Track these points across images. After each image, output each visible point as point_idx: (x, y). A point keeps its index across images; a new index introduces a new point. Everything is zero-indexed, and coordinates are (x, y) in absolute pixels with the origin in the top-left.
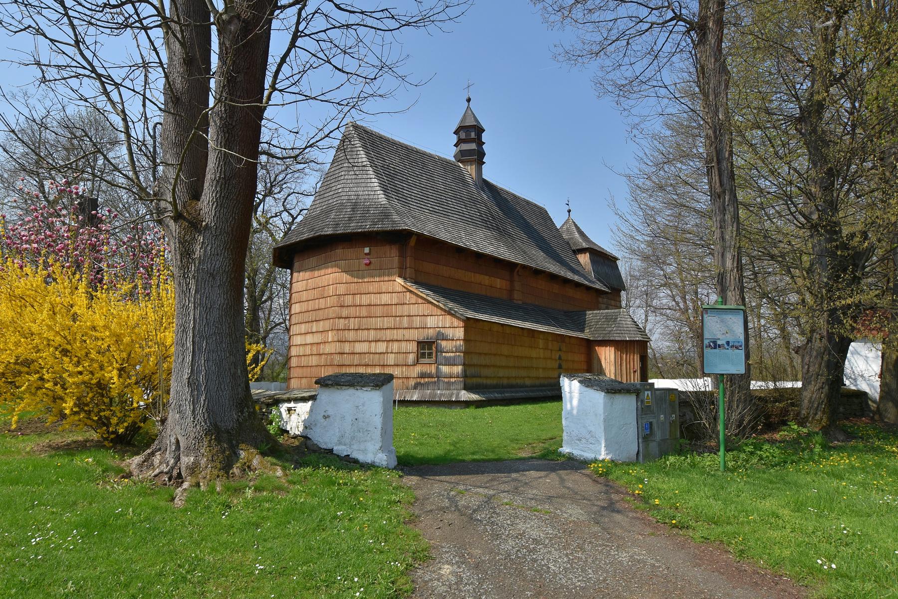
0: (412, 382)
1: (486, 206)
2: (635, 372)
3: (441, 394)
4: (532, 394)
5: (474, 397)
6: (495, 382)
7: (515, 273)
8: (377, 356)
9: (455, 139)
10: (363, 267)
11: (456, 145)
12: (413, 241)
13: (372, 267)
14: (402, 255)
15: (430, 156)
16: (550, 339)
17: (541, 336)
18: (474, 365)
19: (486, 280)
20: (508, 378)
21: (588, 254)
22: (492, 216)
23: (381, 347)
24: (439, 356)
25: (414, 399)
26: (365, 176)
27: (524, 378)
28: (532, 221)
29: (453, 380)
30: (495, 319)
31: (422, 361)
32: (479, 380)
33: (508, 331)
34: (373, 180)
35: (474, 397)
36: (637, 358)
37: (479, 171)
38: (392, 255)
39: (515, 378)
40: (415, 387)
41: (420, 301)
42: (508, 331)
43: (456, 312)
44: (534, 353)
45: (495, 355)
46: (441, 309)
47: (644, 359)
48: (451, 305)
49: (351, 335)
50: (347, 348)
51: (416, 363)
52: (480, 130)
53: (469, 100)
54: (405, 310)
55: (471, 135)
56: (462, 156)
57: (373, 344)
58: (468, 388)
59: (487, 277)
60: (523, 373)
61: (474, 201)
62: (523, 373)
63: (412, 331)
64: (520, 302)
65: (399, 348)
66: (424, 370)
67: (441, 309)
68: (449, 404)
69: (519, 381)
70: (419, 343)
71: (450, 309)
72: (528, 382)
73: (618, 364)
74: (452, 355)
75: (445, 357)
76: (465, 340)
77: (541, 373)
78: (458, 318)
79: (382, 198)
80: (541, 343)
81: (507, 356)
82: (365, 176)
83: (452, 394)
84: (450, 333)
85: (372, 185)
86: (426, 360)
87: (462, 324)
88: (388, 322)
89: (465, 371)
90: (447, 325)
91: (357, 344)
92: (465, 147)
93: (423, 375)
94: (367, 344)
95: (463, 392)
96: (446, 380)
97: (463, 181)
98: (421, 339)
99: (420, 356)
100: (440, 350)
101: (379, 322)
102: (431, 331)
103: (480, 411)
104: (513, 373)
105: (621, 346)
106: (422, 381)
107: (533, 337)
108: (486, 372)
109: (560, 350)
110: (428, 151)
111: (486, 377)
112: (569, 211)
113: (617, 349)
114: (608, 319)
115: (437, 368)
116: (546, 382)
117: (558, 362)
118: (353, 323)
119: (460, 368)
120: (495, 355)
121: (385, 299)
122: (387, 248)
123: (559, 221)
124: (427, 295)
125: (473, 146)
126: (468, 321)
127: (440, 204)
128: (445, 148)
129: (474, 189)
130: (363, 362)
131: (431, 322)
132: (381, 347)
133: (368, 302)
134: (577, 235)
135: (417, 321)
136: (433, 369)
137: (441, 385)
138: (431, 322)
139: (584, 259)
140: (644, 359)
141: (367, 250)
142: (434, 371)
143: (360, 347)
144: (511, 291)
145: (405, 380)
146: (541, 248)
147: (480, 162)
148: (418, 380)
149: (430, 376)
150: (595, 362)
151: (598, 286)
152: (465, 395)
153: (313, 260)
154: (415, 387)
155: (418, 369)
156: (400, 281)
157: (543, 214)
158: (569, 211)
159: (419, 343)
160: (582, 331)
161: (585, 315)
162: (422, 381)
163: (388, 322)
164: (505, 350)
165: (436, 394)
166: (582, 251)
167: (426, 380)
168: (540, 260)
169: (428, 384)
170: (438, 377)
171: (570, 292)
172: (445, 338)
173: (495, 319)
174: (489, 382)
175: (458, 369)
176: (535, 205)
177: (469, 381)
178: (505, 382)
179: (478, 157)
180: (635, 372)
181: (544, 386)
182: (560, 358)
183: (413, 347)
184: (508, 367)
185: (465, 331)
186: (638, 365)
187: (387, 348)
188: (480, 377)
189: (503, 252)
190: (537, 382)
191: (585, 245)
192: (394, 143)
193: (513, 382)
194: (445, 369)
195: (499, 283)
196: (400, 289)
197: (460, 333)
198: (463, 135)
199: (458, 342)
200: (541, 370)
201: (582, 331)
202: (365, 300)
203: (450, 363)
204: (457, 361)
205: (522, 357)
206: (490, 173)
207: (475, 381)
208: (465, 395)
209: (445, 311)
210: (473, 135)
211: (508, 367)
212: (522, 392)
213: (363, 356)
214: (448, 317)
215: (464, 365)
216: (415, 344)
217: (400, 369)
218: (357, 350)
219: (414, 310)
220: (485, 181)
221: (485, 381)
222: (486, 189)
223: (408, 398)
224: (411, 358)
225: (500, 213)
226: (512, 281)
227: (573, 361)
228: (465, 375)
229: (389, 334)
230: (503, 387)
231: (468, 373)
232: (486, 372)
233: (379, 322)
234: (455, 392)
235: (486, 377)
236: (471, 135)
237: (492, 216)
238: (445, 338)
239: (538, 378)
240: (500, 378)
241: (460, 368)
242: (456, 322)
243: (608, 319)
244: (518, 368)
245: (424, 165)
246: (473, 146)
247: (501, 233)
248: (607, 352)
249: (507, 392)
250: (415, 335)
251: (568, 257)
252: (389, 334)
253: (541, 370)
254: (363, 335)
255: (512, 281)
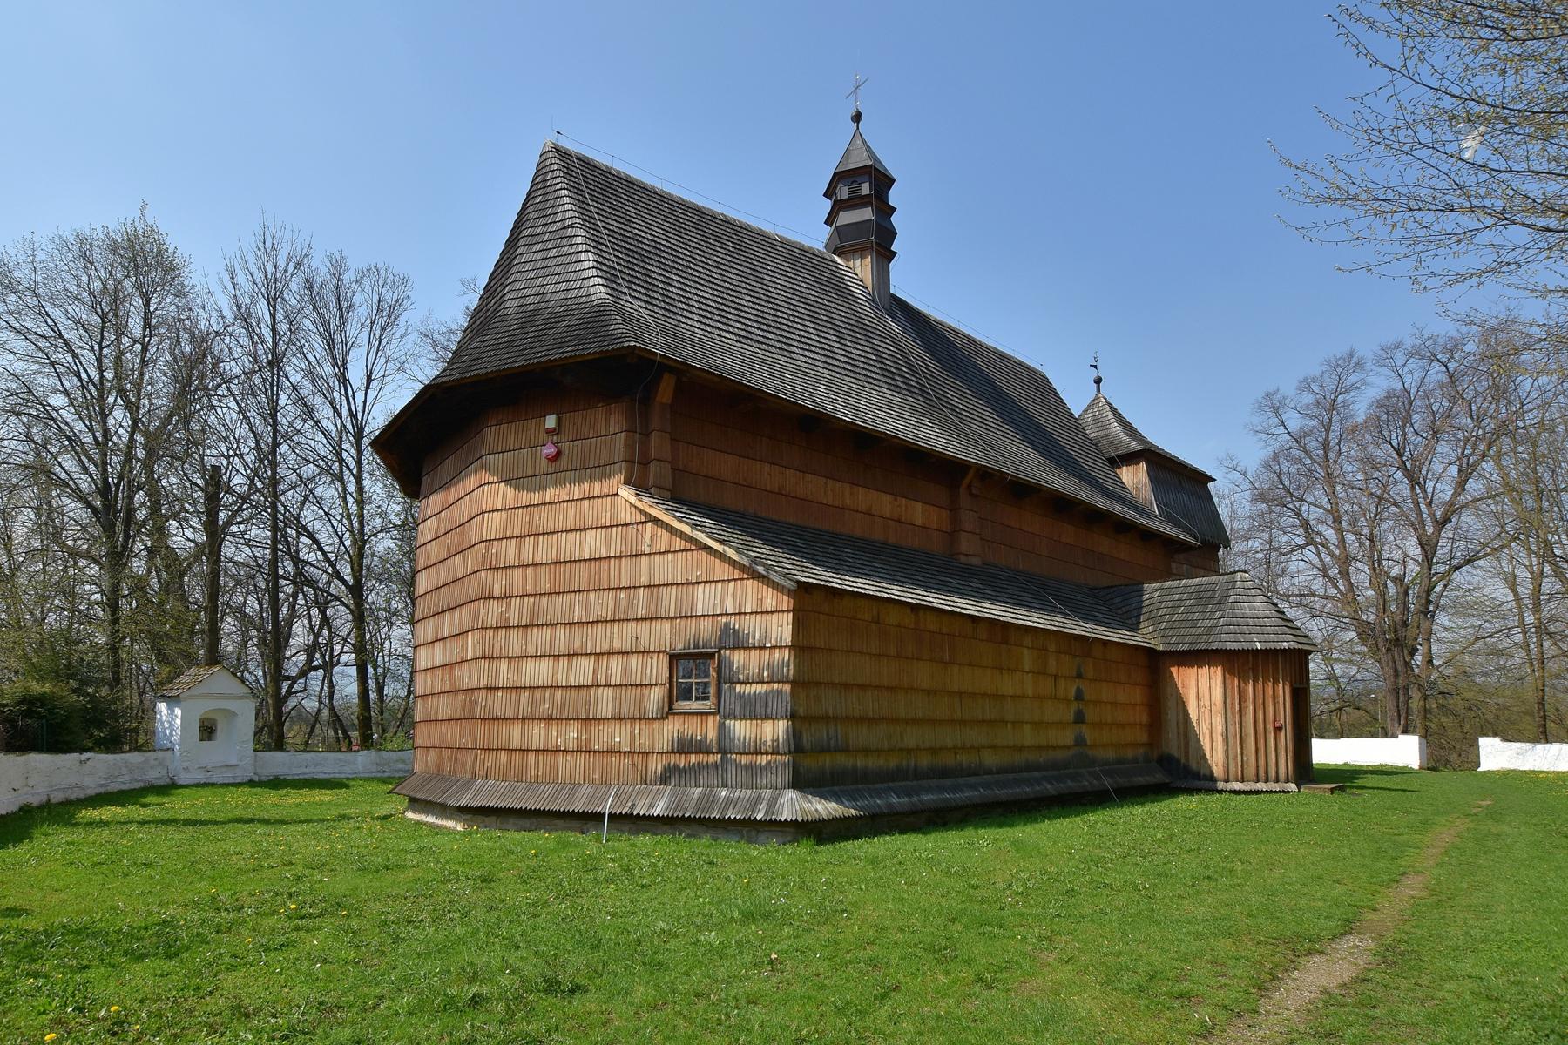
0: (656, 765)
1: (895, 343)
2: (1278, 729)
3: (729, 800)
4: (1000, 793)
5: (823, 808)
6: (893, 763)
7: (962, 490)
8: (573, 693)
9: (827, 205)
10: (543, 466)
11: (829, 222)
12: (665, 391)
13: (563, 463)
14: (639, 429)
15: (761, 236)
16: (1052, 648)
17: (1028, 641)
18: (826, 719)
19: (884, 503)
20: (934, 751)
21: (1143, 466)
22: (910, 366)
23: (582, 671)
24: (726, 695)
25: (658, 810)
26: (566, 250)
27: (980, 749)
28: (1013, 390)
29: (762, 760)
30: (894, 592)
31: (684, 706)
32: (842, 760)
33: (931, 623)
34: (583, 256)
35: (823, 808)
36: (1283, 692)
37: (882, 275)
38: (610, 429)
39: (954, 750)
40: (664, 779)
41: (678, 544)
42: (931, 623)
43: (768, 568)
44: (1008, 685)
45: (891, 689)
46: (733, 563)
47: (1300, 696)
48: (760, 550)
49: (513, 642)
50: (503, 674)
51: (668, 712)
52: (883, 181)
53: (857, 118)
54: (641, 571)
55: (863, 192)
56: (846, 241)
57: (563, 663)
58: (802, 782)
59: (886, 498)
60: (974, 736)
61: (866, 332)
62: (974, 736)
63: (657, 626)
64: (976, 561)
65: (626, 672)
66: (688, 732)
67: (733, 563)
68: (749, 828)
69: (964, 759)
70: (674, 658)
71: (754, 560)
72: (991, 760)
73: (1234, 710)
74: (760, 688)
75: (741, 696)
76: (798, 647)
77: (1028, 737)
78: (777, 587)
79: (598, 290)
80: (1028, 659)
81: (929, 692)
82: (566, 250)
83: (759, 800)
84: (754, 627)
85: (579, 266)
86: (693, 706)
87: (786, 602)
88: (600, 605)
89: (795, 739)
90: (747, 604)
91: (526, 665)
92: (846, 218)
93: (684, 746)
94: (547, 664)
95: (790, 794)
96: (745, 760)
97: (843, 292)
98: (679, 648)
99: (678, 693)
100: (727, 678)
101: (575, 606)
102: (705, 624)
103: (827, 852)
104: (948, 737)
105: (1242, 664)
106: (682, 761)
107: (1005, 641)
108: (861, 736)
109: (1079, 676)
110: (755, 223)
111: (866, 751)
112: (1098, 381)
113: (1229, 670)
114: (1202, 599)
115: (722, 726)
116: (1042, 758)
117: (1074, 707)
118: (518, 610)
119: (782, 725)
120: (891, 689)
121: (593, 544)
122: (600, 412)
123: (1076, 399)
124: (695, 526)
125: (866, 214)
126: (803, 593)
127: (773, 327)
128: (808, 227)
129: (867, 308)
130: (539, 713)
131: (704, 599)
132: (582, 671)
133: (552, 556)
134: (1116, 428)
135: (671, 600)
136: (710, 730)
137: (732, 770)
138: (704, 599)
139: (1135, 478)
140: (1300, 696)
141: (551, 421)
142: (712, 734)
143: (536, 672)
144: (953, 534)
145: (638, 759)
146: (1034, 446)
147: (884, 254)
148: (673, 759)
149: (701, 748)
150: (1171, 704)
151: (1169, 530)
152: (793, 805)
153: (448, 467)
154: (664, 779)
155: (671, 729)
156: (627, 493)
157: (1040, 385)
158: (1098, 381)
159: (674, 658)
160: (1134, 627)
161: (1141, 592)
162: (682, 761)
163: (600, 605)
164: (923, 674)
165: (715, 799)
166: (1130, 458)
167: (693, 759)
168: (1026, 463)
169: (696, 770)
170: (723, 751)
171: (1104, 544)
172: (741, 644)
173: (894, 592)
174: (874, 763)
175: (775, 730)
176: (1021, 364)
177: (810, 763)
178: (925, 761)
179: (878, 241)
180: (1278, 729)
181: (1029, 768)
182: (1079, 696)
183: (658, 669)
184: (933, 722)
185: (799, 625)
186: (1285, 715)
187: (596, 672)
188: (846, 750)
189: (931, 436)
190: (1018, 759)
191: (1134, 446)
192: (665, 198)
193: (948, 760)
194: (741, 729)
195: (918, 513)
196: (625, 515)
197: (781, 628)
198: (843, 192)
199: (777, 654)
200: (1027, 728)
201: (1134, 627)
202: (546, 549)
203: (754, 711)
204: (774, 708)
205: (973, 695)
206: (903, 284)
207: (827, 761)
208: (793, 805)
209: (742, 568)
210: (865, 189)
211: (933, 722)
212: (973, 787)
213: (539, 693)
214: (751, 585)
215: (793, 717)
216: (664, 659)
217: (626, 727)
218: (527, 680)
219: (663, 569)
220: (893, 296)
221: (860, 762)
222: (899, 314)
223: (640, 810)
224: (656, 697)
225: (932, 364)
226: (954, 509)
227: (1114, 704)
228: (796, 746)
229: (602, 637)
230: (918, 774)
231: (807, 740)
232: (861, 736)
233: (575, 606)
234: (768, 793)
235: (866, 751)
236: (863, 192)
237: (910, 366)
238: (741, 644)
239: (1020, 749)
240: (909, 751)
241: (782, 725)
242: (771, 599)
243: (1202, 598)
244: (963, 723)
245: (740, 247)
246: (866, 214)
247: (932, 404)
248: (1204, 682)
249: (929, 790)
250: (662, 635)
251: (1099, 470)
252: (602, 637)
253: (1027, 728)
254: (541, 639)
255: (954, 509)
